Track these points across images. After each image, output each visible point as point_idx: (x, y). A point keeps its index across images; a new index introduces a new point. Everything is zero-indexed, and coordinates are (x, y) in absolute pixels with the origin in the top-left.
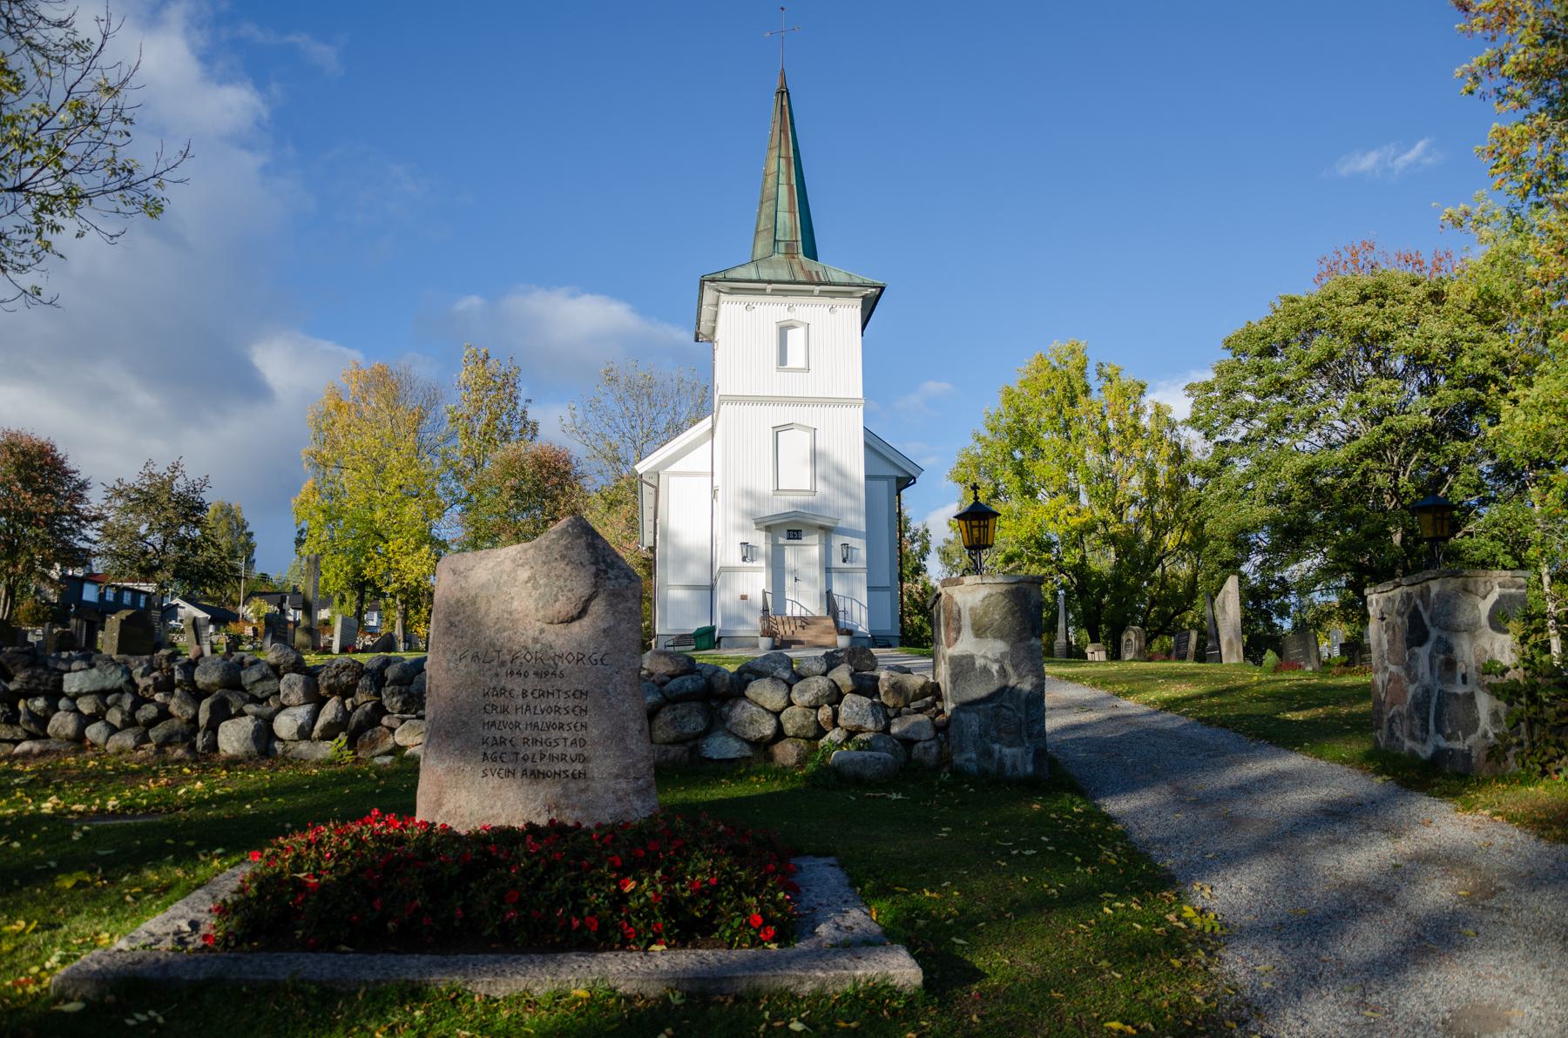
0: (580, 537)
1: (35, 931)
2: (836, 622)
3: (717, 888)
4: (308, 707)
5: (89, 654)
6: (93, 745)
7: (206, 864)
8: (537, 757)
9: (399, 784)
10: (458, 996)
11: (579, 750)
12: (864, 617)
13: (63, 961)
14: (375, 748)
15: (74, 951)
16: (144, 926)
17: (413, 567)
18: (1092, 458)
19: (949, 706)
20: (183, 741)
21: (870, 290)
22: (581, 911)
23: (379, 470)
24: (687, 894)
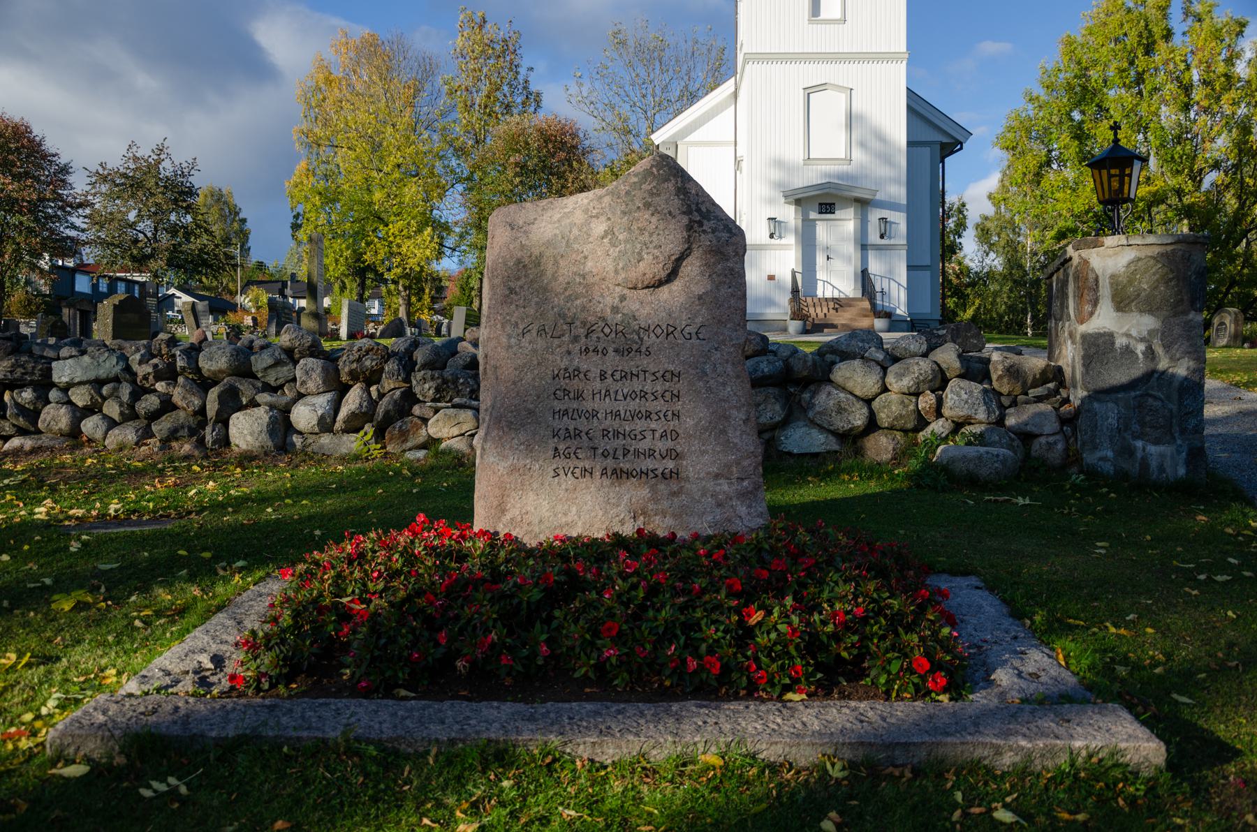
0: (667, 180)
1: (29, 665)
2: (873, 305)
3: (865, 621)
4: (328, 396)
5: (81, 342)
6: (90, 440)
7: (226, 580)
8: (620, 453)
9: (450, 485)
10: (555, 760)
11: (670, 444)
12: (903, 295)
13: (62, 706)
14: (405, 441)
15: (74, 692)
16: (158, 661)
17: (416, 250)
18: (1168, 116)
19: (1078, 395)
20: (191, 436)
22: (697, 648)
23: (376, 147)
24: (830, 628)
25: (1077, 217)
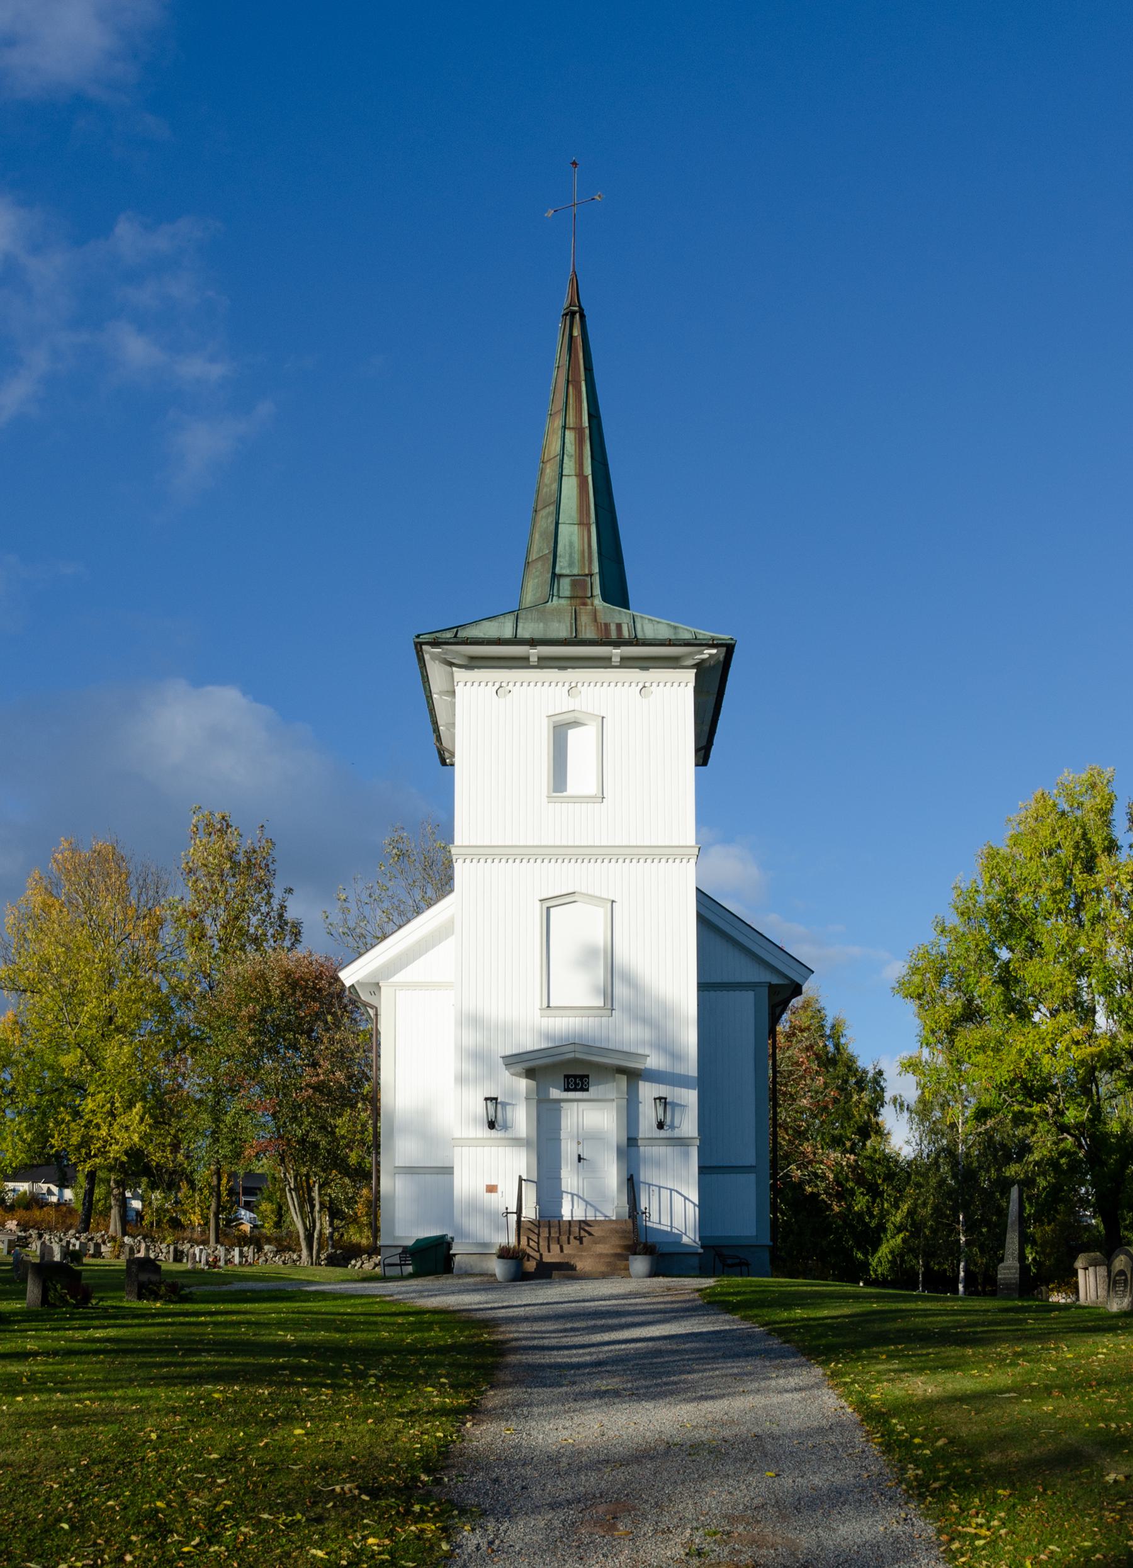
12: (692, 1212)
21: (709, 652)
25: (1000, 1088)
